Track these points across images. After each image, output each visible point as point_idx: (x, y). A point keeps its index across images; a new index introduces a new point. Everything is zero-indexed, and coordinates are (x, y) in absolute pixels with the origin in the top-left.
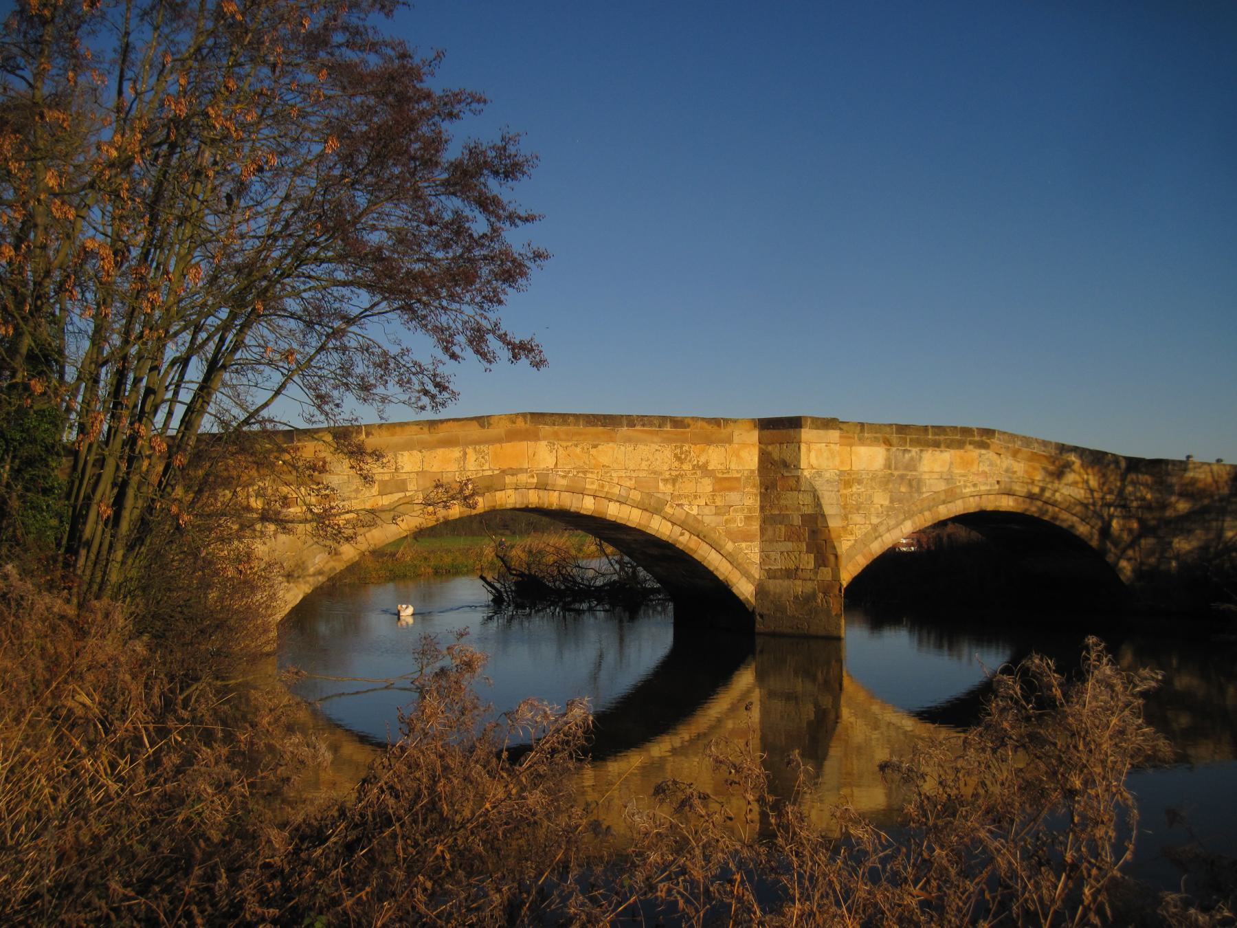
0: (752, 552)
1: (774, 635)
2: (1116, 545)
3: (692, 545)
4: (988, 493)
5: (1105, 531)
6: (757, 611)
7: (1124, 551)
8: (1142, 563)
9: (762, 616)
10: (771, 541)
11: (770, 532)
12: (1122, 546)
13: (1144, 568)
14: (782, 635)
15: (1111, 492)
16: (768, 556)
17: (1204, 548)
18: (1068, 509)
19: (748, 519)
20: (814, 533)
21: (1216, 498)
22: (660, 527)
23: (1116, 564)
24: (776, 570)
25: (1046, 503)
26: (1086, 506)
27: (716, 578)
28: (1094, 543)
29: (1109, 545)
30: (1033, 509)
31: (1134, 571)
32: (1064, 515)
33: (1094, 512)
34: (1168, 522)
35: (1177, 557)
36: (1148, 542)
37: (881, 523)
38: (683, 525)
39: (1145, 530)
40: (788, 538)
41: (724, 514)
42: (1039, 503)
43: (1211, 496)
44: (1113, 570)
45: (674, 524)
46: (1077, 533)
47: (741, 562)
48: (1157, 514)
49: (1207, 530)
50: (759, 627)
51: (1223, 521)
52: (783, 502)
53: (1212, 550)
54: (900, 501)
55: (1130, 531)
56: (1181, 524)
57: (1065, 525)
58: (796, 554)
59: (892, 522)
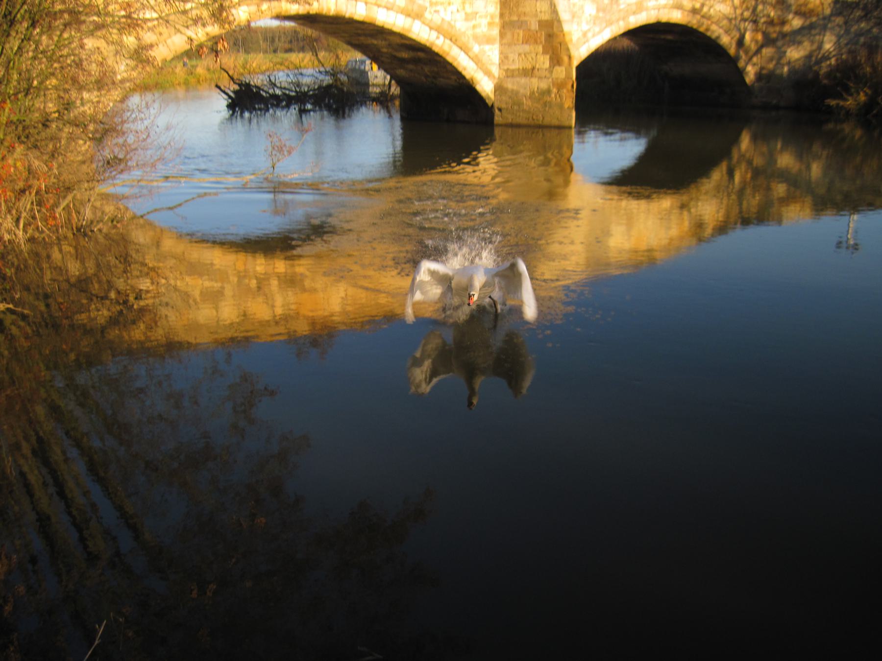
0: (492, 53)
1: (512, 126)
2: (746, 52)
3: (446, 48)
4: (665, 7)
5: (740, 43)
6: (496, 105)
7: (750, 59)
8: (762, 68)
9: (500, 110)
10: (510, 45)
11: (509, 36)
12: (751, 53)
13: (764, 72)
14: (519, 126)
15: (747, 9)
16: (506, 58)
17: (809, 57)
18: (717, 23)
19: (490, 24)
20: (550, 36)
21: (821, 16)
22: (420, 33)
23: (745, 69)
24: (513, 71)
25: (703, 17)
26: (730, 20)
27: (463, 77)
28: (732, 51)
29: (742, 53)
30: (693, 21)
31: (756, 74)
32: (714, 27)
33: (735, 25)
34: (784, 35)
35: (789, 63)
36: (767, 51)
37: (589, 30)
38: (439, 30)
39: (768, 41)
40: (526, 41)
41: (472, 19)
42: (698, 17)
43: (818, 15)
44: (741, 73)
45: (431, 28)
46: (721, 43)
47: (484, 66)
48: (777, 29)
49: (812, 42)
50: (498, 118)
51: (824, 35)
52: (521, 9)
53: (814, 59)
54: (604, 11)
55: (757, 42)
56: (794, 38)
57: (713, 37)
58: (534, 55)
59: (597, 29)
